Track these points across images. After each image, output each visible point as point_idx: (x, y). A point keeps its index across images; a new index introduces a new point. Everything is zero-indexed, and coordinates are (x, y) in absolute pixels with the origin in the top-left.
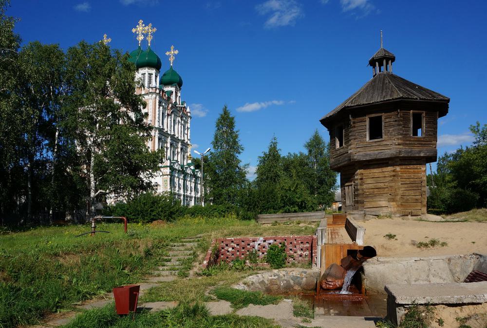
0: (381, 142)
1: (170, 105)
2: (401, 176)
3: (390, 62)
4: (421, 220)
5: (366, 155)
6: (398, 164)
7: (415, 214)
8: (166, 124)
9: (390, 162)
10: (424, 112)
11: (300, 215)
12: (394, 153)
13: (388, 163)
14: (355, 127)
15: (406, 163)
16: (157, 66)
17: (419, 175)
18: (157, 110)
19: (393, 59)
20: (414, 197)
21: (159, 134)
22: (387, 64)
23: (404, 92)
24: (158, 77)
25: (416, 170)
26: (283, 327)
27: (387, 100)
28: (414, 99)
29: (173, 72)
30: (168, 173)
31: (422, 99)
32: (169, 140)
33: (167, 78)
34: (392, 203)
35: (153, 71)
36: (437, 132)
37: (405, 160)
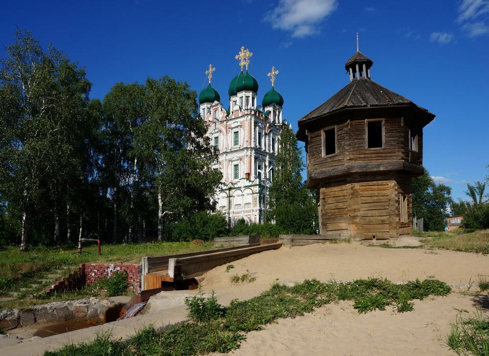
0: (335, 157)
1: (268, 124)
2: (362, 194)
4: (387, 246)
5: (322, 172)
6: (358, 180)
7: (381, 237)
8: (264, 143)
9: (348, 179)
10: (384, 119)
11: (235, 239)
12: (346, 169)
13: (346, 180)
15: (368, 179)
16: (254, 88)
17: (385, 192)
18: (253, 130)
19: (369, 64)
20: (379, 217)
21: (255, 153)
24: (256, 99)
25: (382, 187)
26: (174, 355)
27: (341, 108)
29: (273, 91)
30: (258, 191)
32: (267, 159)
33: (269, 99)
34: (351, 226)
35: (250, 94)
36: (422, 143)
37: (366, 175)
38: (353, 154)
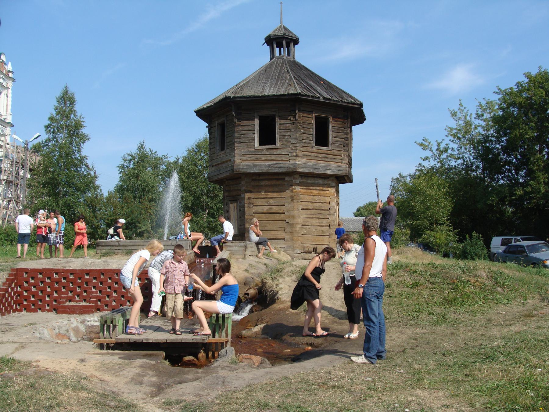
3: (292, 44)
5: (255, 166)
12: (291, 166)
13: (284, 179)
14: (239, 126)
17: (326, 198)
19: (296, 42)
22: (288, 46)
23: (305, 88)
28: (316, 97)
31: (327, 99)
38: (300, 151)
